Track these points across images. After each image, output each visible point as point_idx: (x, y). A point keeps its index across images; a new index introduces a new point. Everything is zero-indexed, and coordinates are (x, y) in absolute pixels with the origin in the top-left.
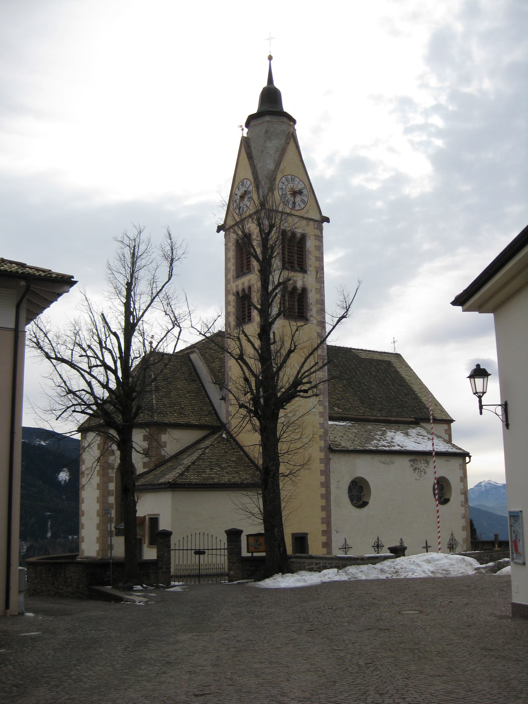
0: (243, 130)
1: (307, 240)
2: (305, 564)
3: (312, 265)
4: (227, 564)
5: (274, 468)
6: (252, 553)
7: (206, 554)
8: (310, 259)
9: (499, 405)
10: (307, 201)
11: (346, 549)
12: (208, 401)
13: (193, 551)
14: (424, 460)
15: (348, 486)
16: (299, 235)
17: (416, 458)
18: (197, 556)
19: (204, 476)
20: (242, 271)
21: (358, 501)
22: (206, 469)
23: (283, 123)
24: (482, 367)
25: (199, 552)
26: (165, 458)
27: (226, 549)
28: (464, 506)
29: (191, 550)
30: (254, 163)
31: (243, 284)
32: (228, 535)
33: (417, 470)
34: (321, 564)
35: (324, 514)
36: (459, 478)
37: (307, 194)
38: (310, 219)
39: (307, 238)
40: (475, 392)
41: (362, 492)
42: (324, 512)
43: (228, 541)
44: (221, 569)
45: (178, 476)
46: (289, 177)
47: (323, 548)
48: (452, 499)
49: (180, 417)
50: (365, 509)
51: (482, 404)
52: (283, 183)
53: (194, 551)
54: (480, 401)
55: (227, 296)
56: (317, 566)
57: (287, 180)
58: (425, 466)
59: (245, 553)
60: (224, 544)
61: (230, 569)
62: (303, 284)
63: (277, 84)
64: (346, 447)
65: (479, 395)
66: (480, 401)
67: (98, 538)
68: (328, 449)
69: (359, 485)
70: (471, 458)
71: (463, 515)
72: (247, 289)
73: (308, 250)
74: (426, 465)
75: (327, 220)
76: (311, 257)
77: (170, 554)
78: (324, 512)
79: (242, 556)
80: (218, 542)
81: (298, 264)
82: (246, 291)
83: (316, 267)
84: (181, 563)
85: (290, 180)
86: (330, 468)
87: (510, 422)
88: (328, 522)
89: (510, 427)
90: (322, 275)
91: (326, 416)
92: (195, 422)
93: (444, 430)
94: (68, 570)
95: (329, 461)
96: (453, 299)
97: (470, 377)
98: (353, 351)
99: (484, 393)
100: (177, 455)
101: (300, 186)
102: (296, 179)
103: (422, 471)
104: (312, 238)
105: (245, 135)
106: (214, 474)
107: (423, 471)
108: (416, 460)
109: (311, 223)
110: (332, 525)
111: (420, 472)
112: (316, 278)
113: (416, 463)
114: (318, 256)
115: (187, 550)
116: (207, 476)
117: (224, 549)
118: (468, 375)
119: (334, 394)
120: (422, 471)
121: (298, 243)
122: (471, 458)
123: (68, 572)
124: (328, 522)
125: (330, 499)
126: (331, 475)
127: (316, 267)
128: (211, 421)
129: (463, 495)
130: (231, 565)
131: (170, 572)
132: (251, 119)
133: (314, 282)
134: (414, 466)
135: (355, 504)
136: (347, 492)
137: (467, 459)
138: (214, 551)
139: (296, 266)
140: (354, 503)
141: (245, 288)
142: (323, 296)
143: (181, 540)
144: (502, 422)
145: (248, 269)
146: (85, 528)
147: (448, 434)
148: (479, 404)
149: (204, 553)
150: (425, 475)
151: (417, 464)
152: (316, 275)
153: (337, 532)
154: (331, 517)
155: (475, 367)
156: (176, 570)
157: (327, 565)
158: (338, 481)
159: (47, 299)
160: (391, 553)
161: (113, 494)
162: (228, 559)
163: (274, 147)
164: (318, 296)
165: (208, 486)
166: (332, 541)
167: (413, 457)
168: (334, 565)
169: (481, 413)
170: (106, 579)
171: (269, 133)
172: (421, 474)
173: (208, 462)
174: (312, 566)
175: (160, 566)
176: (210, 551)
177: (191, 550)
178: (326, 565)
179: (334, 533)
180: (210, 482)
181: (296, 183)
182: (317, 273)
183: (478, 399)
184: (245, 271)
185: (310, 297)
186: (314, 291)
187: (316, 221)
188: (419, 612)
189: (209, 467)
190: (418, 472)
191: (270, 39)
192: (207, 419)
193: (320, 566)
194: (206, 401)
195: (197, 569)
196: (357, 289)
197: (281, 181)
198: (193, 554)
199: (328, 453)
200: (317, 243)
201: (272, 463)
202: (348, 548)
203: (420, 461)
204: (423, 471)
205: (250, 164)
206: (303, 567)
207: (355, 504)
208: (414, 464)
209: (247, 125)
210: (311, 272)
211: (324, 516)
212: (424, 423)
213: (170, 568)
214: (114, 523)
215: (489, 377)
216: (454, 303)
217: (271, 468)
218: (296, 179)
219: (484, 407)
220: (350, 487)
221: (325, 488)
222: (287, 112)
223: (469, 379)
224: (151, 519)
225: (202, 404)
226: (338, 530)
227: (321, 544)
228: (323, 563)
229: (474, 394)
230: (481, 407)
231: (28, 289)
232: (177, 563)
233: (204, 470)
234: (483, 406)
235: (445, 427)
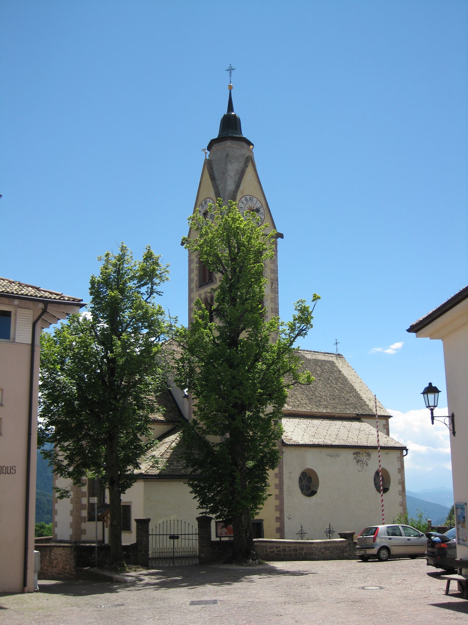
0: (206, 153)
2: (267, 547)
4: (198, 547)
5: (241, 462)
6: (220, 537)
7: (180, 539)
8: (266, 271)
9: (447, 417)
11: (302, 534)
12: (171, 398)
13: (168, 536)
14: (366, 453)
17: (359, 451)
18: (172, 540)
19: (172, 467)
20: (204, 281)
21: (307, 491)
22: (173, 461)
24: (433, 385)
25: (173, 537)
27: (197, 534)
28: (402, 494)
29: (167, 535)
30: (216, 183)
31: (206, 293)
32: (198, 522)
33: (360, 463)
34: (281, 548)
36: (397, 470)
40: (428, 405)
41: (311, 483)
42: (278, 501)
43: (198, 527)
44: (189, 552)
45: (149, 468)
46: (248, 197)
47: (276, 533)
48: (391, 488)
50: (314, 497)
51: (434, 416)
53: (169, 536)
54: (432, 413)
55: (191, 303)
56: (277, 550)
57: (246, 200)
58: (367, 459)
59: (214, 538)
60: (196, 529)
61: (200, 551)
63: (236, 112)
64: (297, 441)
65: (431, 408)
66: (432, 413)
67: (71, 524)
68: (281, 444)
69: (308, 476)
70: (408, 451)
71: (401, 503)
72: (210, 298)
74: (368, 458)
75: (281, 236)
77: (148, 539)
78: (278, 501)
79: (212, 540)
82: (209, 300)
83: (271, 279)
84: (158, 546)
85: (249, 200)
87: (456, 430)
88: (281, 510)
89: (456, 434)
90: (276, 286)
92: (160, 418)
93: (383, 425)
94: (54, 553)
96: (408, 327)
97: (423, 393)
99: (435, 406)
101: (258, 205)
103: (364, 463)
105: (208, 158)
106: (180, 466)
107: (365, 463)
108: (359, 453)
110: (285, 512)
111: (363, 464)
113: (359, 456)
114: (273, 268)
115: (159, 535)
116: (175, 468)
117: (196, 534)
118: (422, 392)
120: (364, 463)
122: (408, 451)
123: (54, 554)
124: (281, 510)
125: (283, 489)
126: (284, 467)
127: (271, 279)
128: (174, 417)
129: (401, 485)
130: (202, 548)
131: (148, 554)
132: (212, 143)
133: (270, 292)
135: (305, 493)
136: (298, 482)
137: (405, 452)
138: (191, 536)
140: (304, 492)
141: (208, 297)
142: (277, 305)
143: (158, 526)
144: (450, 430)
145: (210, 280)
146: (58, 514)
147: (386, 429)
148: (431, 416)
149: (177, 538)
150: (367, 467)
153: (289, 518)
154: (284, 505)
155: (428, 385)
156: (153, 553)
157: (286, 548)
158: (290, 473)
159: (55, 317)
160: (341, 538)
162: (199, 543)
163: (235, 169)
164: (272, 305)
165: (176, 477)
166: (285, 527)
167: (357, 450)
168: (292, 549)
169: (433, 423)
170: (91, 561)
171: (230, 157)
172: (363, 465)
173: (175, 455)
174: (273, 550)
175: (139, 549)
176: (183, 536)
177: (167, 535)
178: (285, 548)
179: (286, 519)
180: (178, 473)
181: (254, 202)
182: (272, 284)
183: (430, 411)
184: (207, 281)
185: (266, 306)
186: (269, 300)
188: (379, 588)
189: (176, 459)
190: (361, 464)
191: (230, 70)
192: (171, 415)
193: (280, 550)
194: (169, 398)
195: (172, 552)
196: (315, 305)
198: (168, 539)
199: (281, 447)
201: (240, 458)
202: (304, 533)
203: (362, 454)
204: (365, 463)
205: (213, 185)
206: (265, 551)
207: (305, 493)
208: (357, 456)
209: (209, 148)
212: (365, 418)
213: (148, 551)
214: (87, 509)
215: (439, 393)
216: (409, 331)
217: (239, 463)
219: (435, 418)
222: (246, 137)
223: (423, 394)
225: (166, 401)
226: (290, 517)
227: (275, 529)
228: (283, 547)
229: (427, 407)
230: (433, 418)
231: (44, 311)
232: (154, 546)
233: (171, 462)
234: (435, 418)
235: (384, 422)
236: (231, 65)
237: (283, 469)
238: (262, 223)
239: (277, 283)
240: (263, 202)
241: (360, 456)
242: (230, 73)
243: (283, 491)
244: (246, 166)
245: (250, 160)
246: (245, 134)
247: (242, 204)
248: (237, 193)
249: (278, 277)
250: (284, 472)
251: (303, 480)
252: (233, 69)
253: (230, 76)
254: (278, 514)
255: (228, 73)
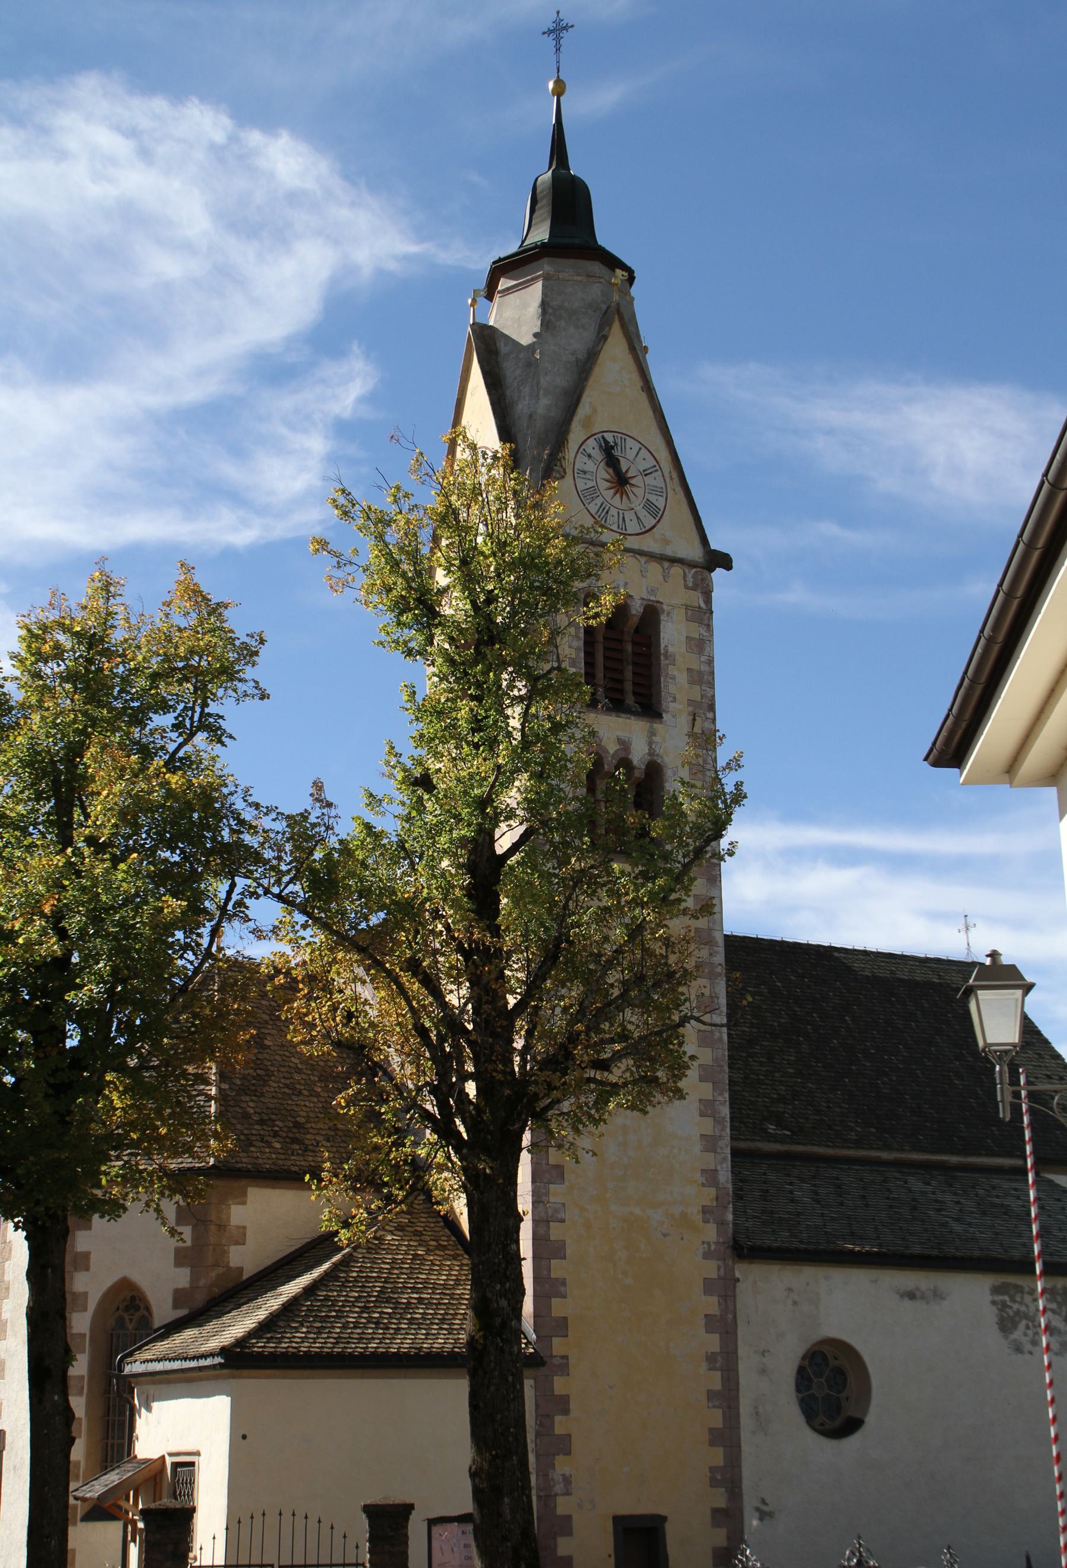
1: (663, 623)
3: (678, 696)
8: (674, 678)
10: (661, 507)
15: (795, 1369)
16: (637, 608)
23: (591, 280)
26: (241, 1275)
33: (1024, 1323)
35: (717, 1456)
37: (664, 486)
38: (674, 561)
39: (663, 617)
42: (720, 1451)
49: (289, 1152)
50: (853, 1443)
52: (589, 456)
62: (651, 753)
73: (667, 652)
75: (724, 561)
76: (676, 673)
78: (720, 1451)
80: (338, 1540)
81: (635, 693)
83: (691, 702)
86: (735, 1308)
91: (721, 1148)
95: (735, 1287)
98: (836, 954)
100: (277, 1269)
102: (630, 443)
104: (679, 615)
109: (677, 570)
112: (691, 735)
114: (695, 667)
119: (767, 1084)
121: (637, 630)
126: (739, 1329)
127: (691, 702)
134: (1011, 1307)
135: (822, 1424)
136: (793, 1387)
139: (630, 700)
151: (1021, 1303)
152: (690, 725)
158: (763, 1353)
161: (82, 1388)
171: (550, 311)
182: (694, 720)
187: (692, 565)
190: (1028, 1327)
197: (581, 450)
200: (697, 630)
207: (822, 1424)
208: (1013, 1300)
210: (674, 716)
211: (720, 1462)
218: (630, 443)
220: (801, 1371)
221: (720, 1372)
224: (176, 1465)
236: (558, 13)
237: (736, 1339)
238: (658, 522)
239: (710, 715)
240: (663, 455)
241: (1022, 1298)
242: (558, 39)
243: (738, 1415)
244: (602, 338)
245: (616, 316)
246: (603, 239)
247: (586, 459)
248: (570, 424)
249: (714, 695)
250: (743, 1351)
251: (815, 1380)
252: (566, 28)
253: (558, 50)
254: (721, 1501)
255: (550, 41)
